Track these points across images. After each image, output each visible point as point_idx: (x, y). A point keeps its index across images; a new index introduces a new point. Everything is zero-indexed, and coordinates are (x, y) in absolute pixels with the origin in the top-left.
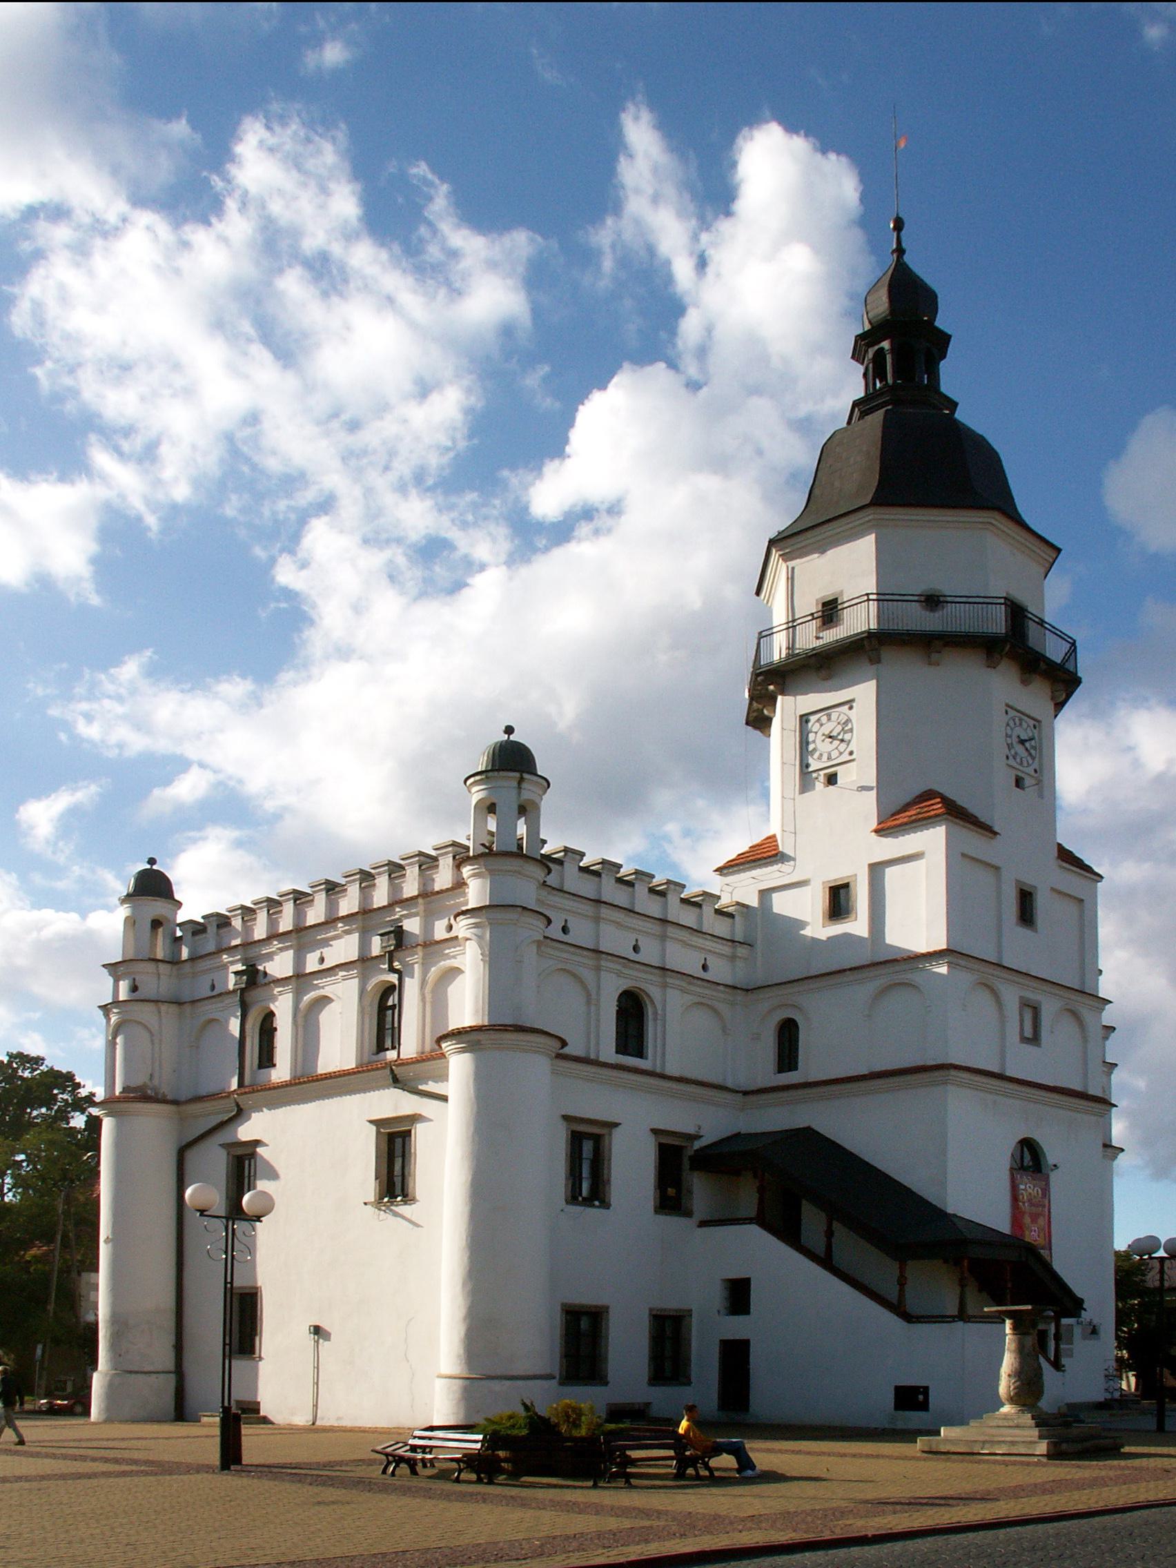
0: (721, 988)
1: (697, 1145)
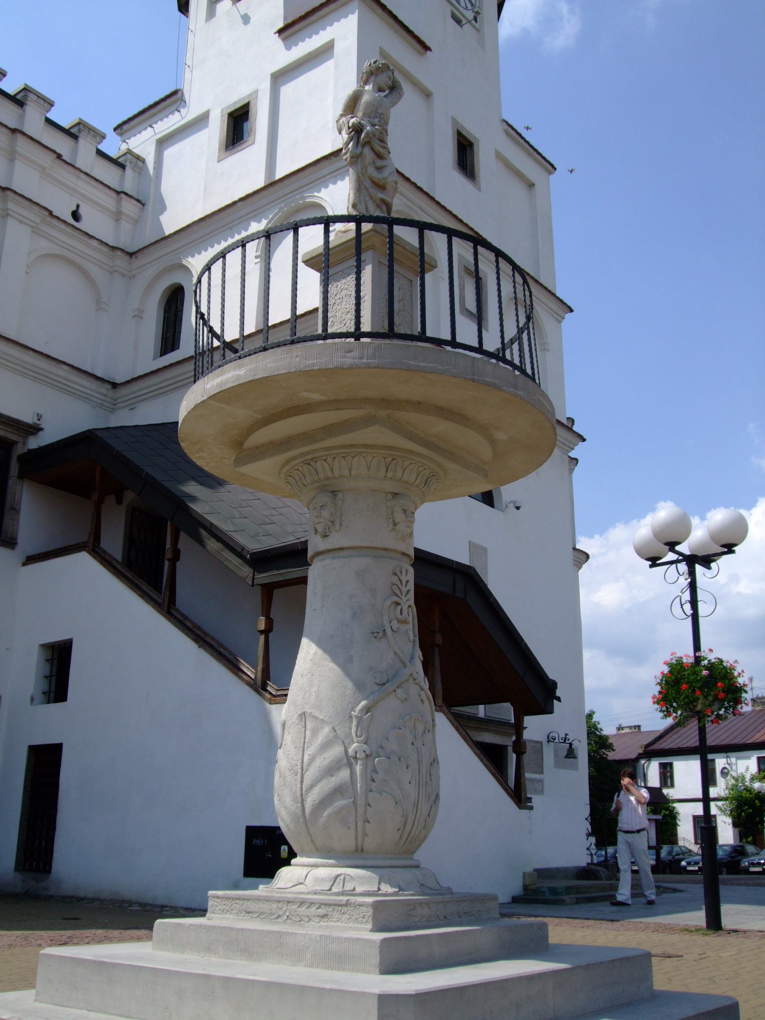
0: (95, 243)
1: (34, 443)
